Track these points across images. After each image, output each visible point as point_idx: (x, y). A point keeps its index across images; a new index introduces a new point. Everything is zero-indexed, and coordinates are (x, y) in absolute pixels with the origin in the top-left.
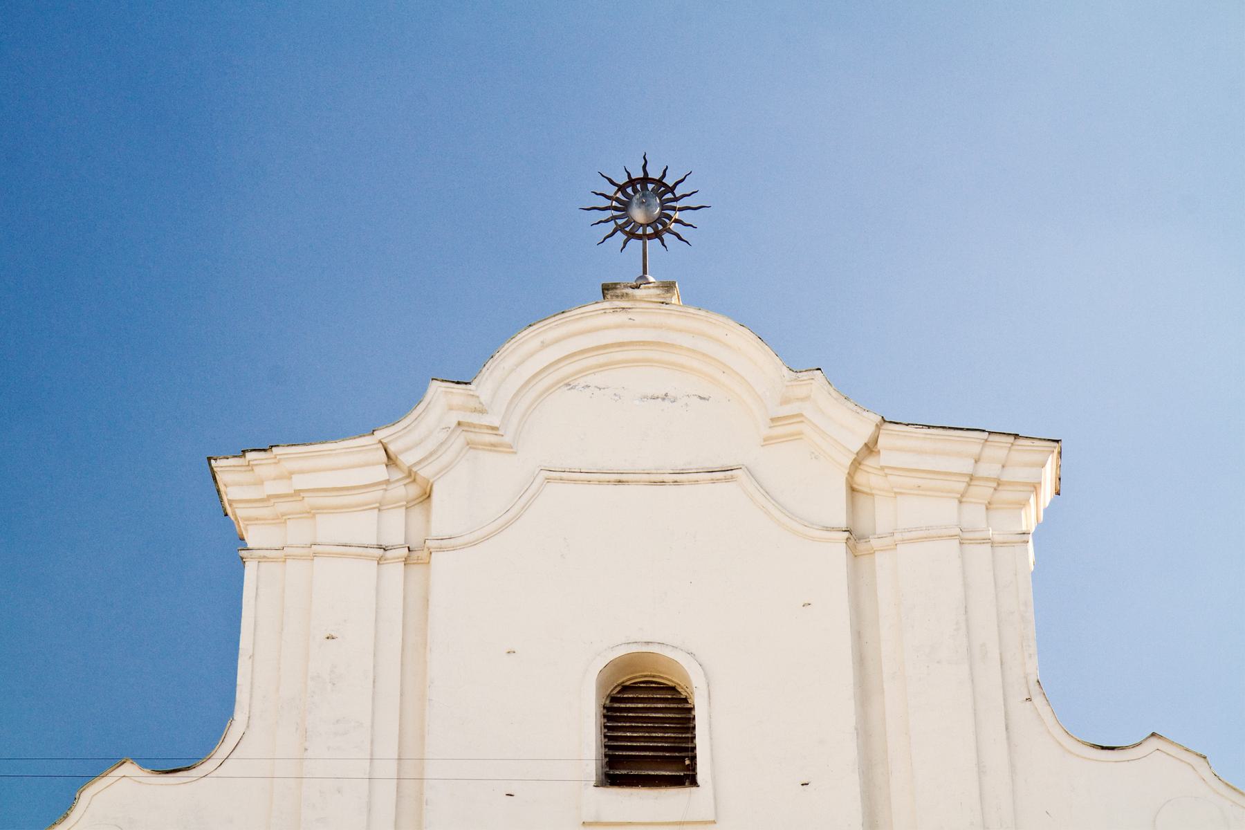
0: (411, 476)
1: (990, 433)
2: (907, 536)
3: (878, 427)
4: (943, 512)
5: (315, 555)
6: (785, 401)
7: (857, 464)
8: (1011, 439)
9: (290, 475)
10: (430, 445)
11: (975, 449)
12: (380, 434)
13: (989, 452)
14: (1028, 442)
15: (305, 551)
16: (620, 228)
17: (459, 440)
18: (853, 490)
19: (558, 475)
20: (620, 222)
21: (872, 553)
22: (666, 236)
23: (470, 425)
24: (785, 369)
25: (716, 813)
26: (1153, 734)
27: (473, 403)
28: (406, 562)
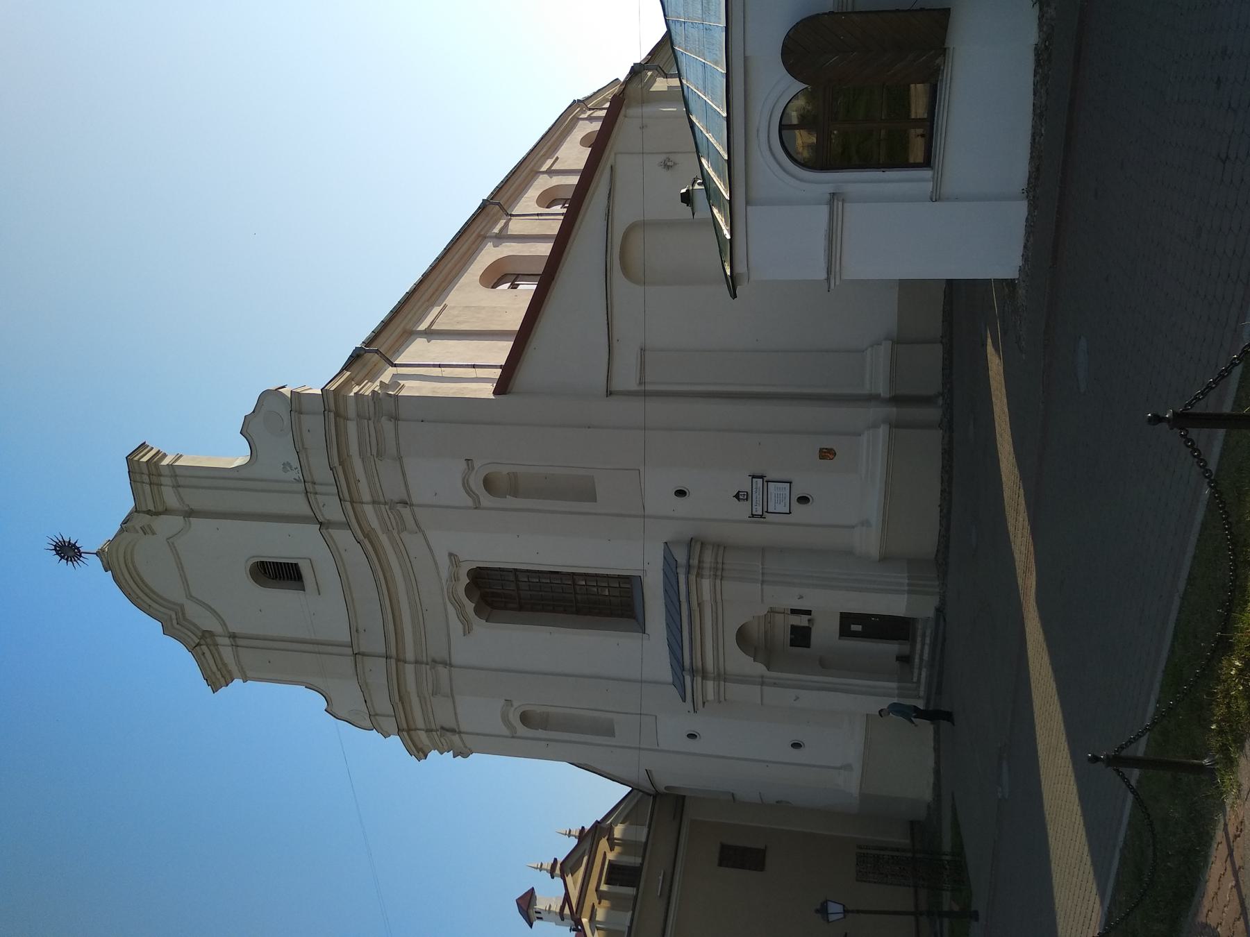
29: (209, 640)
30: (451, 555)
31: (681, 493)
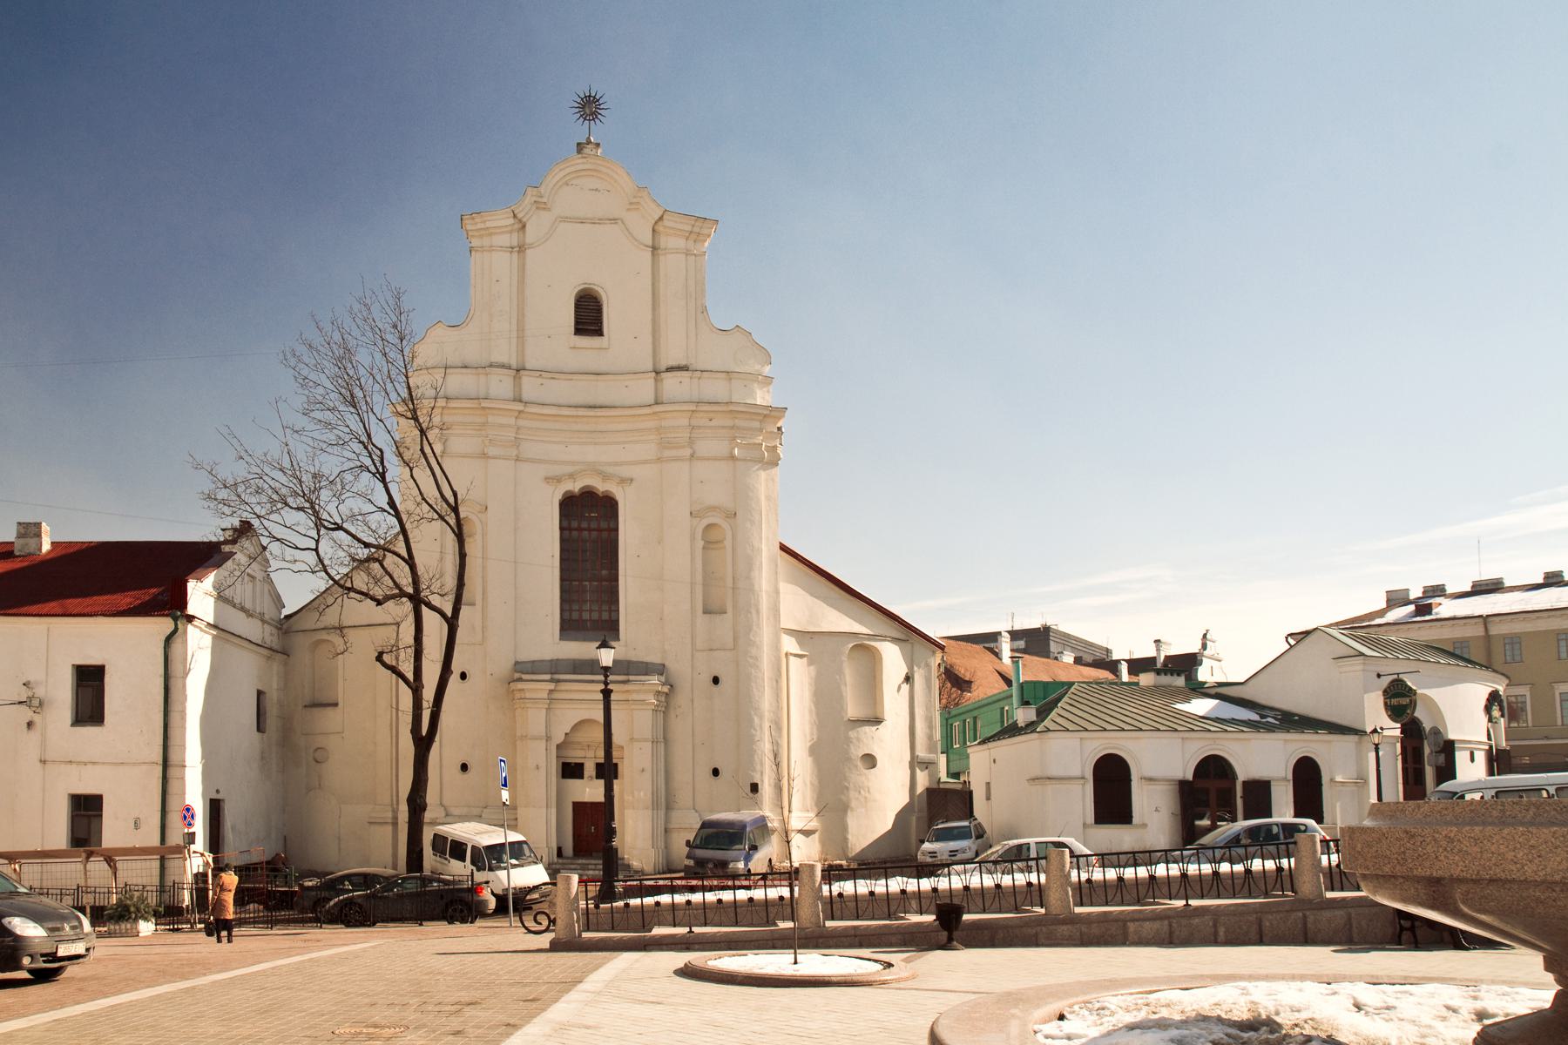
0: (520, 221)
4: (680, 243)
6: (635, 197)
7: (656, 223)
9: (485, 222)
11: (693, 223)
17: (534, 208)
18: (654, 230)
19: (565, 219)
22: (596, 120)
25: (609, 345)
28: (519, 252)
29: (516, 226)
30: (632, 480)
31: (716, 680)
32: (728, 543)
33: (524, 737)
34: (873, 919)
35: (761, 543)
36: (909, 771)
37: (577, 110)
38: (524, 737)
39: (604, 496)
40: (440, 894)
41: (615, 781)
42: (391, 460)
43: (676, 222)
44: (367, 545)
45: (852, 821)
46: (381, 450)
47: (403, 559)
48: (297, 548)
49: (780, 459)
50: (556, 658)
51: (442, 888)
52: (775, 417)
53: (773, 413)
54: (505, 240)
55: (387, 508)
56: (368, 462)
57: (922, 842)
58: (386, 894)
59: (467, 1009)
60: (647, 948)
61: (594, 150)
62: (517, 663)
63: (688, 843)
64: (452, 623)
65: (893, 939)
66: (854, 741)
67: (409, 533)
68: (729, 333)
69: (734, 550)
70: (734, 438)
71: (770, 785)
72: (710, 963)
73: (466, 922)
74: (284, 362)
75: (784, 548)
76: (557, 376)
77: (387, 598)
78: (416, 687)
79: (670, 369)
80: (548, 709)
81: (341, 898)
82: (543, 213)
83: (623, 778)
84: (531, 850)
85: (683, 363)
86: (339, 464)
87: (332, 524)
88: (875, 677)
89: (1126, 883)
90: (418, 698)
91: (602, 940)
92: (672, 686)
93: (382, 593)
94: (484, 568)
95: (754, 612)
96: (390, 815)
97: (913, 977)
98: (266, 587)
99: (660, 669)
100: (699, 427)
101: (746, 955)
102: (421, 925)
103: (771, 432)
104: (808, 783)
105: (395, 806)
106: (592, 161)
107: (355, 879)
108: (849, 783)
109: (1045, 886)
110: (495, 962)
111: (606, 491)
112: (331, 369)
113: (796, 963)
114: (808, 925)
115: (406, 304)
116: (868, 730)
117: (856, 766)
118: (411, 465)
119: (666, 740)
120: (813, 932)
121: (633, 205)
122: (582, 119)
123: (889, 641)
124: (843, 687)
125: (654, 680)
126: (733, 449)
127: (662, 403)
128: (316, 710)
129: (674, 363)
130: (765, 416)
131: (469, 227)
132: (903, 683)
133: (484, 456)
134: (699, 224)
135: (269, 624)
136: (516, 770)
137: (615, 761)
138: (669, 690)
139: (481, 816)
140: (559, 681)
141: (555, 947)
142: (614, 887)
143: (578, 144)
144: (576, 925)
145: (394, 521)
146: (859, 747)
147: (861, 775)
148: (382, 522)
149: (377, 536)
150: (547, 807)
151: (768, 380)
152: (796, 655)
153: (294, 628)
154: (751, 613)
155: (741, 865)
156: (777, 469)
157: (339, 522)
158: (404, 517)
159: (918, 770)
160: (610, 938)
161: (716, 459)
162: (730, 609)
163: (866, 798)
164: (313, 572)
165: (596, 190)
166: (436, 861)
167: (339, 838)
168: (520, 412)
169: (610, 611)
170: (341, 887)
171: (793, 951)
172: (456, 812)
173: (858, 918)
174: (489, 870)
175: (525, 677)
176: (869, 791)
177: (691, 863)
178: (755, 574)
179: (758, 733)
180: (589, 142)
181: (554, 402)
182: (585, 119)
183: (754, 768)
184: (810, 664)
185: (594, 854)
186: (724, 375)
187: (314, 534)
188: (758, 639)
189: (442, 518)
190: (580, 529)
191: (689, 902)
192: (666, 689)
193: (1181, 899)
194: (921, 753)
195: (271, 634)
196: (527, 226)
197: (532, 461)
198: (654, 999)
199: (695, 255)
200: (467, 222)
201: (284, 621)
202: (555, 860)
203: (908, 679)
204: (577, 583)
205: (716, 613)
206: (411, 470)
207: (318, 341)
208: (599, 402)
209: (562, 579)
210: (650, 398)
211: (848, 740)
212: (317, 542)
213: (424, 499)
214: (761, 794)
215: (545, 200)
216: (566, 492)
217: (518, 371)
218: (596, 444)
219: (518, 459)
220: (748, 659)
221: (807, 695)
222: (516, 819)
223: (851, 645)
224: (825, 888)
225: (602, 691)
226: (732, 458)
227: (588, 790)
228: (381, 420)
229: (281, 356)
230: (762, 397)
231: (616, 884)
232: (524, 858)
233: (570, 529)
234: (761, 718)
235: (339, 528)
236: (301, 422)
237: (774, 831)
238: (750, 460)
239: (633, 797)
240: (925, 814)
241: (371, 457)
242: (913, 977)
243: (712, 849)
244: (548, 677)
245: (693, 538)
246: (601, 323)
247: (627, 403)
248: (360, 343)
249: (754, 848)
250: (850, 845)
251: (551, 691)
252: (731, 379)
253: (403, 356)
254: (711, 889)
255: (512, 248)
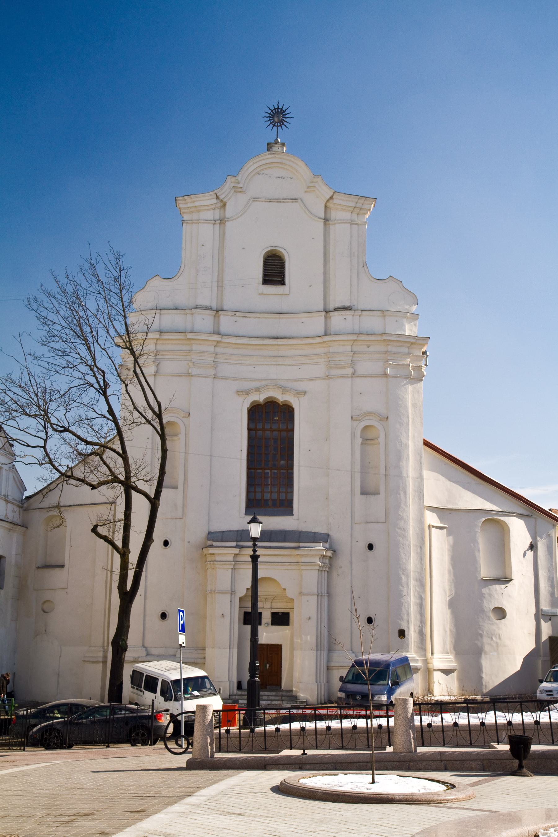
0: (222, 201)
1: (360, 196)
2: (338, 222)
3: (334, 193)
4: (347, 215)
5: (200, 223)
6: (312, 182)
7: (328, 201)
8: (365, 198)
9: (194, 202)
10: (226, 193)
12: (216, 191)
13: (360, 201)
14: (369, 199)
15: (196, 222)
16: (271, 123)
17: (233, 191)
19: (257, 199)
20: (271, 121)
21: (329, 224)
22: (283, 126)
23: (236, 187)
24: (312, 175)
25: (386, 520)
26: (391, 276)
27: (237, 181)
28: (220, 224)
30: (305, 392)
31: (370, 547)
32: (381, 440)
33: (213, 592)
34: (457, 746)
35: (408, 440)
36: (535, 623)
37: (268, 119)
38: (213, 592)
39: (283, 405)
40: (126, 721)
41: (259, 627)
42: (111, 378)
43: (343, 200)
44: (87, 443)
45: (485, 663)
46: (103, 372)
47: (118, 453)
48: (29, 446)
49: (424, 376)
50: (241, 529)
51: (126, 715)
52: (419, 344)
53: (418, 342)
54: (209, 215)
55: (107, 415)
56: (93, 380)
57: (541, 681)
58: (80, 721)
59: (79, 819)
60: (267, 767)
61: (280, 149)
62: (210, 533)
63: (341, 679)
64: (154, 503)
65: (474, 764)
66: (487, 596)
67: (123, 434)
68: (385, 281)
69: (386, 445)
70: (387, 361)
71: (415, 632)
72: (302, 781)
73: (147, 745)
74: (29, 306)
75: (427, 444)
76: (247, 315)
77: (101, 484)
78: (124, 553)
79: (336, 309)
80: (233, 569)
81: (43, 725)
82: (239, 195)
83: (293, 625)
84: (211, 684)
85: (347, 304)
86: (69, 382)
87: (61, 427)
88: (503, 545)
89: (487, 727)
90: (125, 562)
91: (230, 760)
92: (334, 551)
93: (97, 480)
94: (186, 460)
95: (402, 493)
96: (101, 654)
97: (470, 798)
98: (11, 475)
99: (325, 538)
100: (359, 352)
101: (337, 775)
102: (108, 747)
103: (417, 356)
104: (448, 630)
105: (106, 648)
106: (279, 156)
107: (63, 709)
108: (483, 631)
109: (393, 728)
110: (130, 779)
111: (286, 401)
112: (64, 311)
113: (373, 782)
114: (402, 750)
115: (125, 263)
116: (498, 588)
117: (489, 617)
118: (126, 383)
119: (329, 594)
120: (405, 756)
121: (310, 189)
122: (271, 126)
123: (515, 516)
124: (477, 553)
125: (320, 546)
126: (387, 368)
127: (330, 335)
128: (46, 571)
129: (340, 305)
130: (412, 343)
131: (181, 206)
132: (528, 550)
133: (189, 375)
134: (361, 201)
135: (12, 503)
136: (206, 618)
137: (260, 610)
138: (333, 554)
139: (175, 656)
140: (242, 547)
141: (191, 766)
142: (255, 715)
143: (268, 144)
144: (210, 747)
145: (111, 424)
146: (491, 602)
147: (493, 624)
148: (104, 425)
149: (99, 436)
150: (230, 649)
151: (415, 316)
152: (437, 527)
153: (33, 507)
154: (399, 494)
155: (384, 698)
156: (421, 385)
157: (66, 425)
158: (120, 422)
159: (542, 622)
160: (237, 758)
161: (372, 376)
162: (382, 490)
163: (497, 643)
164: (40, 464)
165: (282, 177)
166: (133, 693)
167: (58, 675)
168: (218, 342)
169: (287, 492)
170: (52, 715)
171: (371, 772)
172: (154, 651)
173: (444, 745)
174: (174, 700)
175: (215, 544)
176: (500, 638)
177: (343, 695)
178: (403, 464)
179: (405, 589)
180: (276, 142)
181: (245, 334)
182: (274, 125)
183: (402, 617)
184: (449, 534)
185: (268, 687)
186: (379, 313)
187: (43, 435)
188: (405, 514)
189: (149, 422)
190: (264, 430)
191: (354, 727)
192: (329, 554)
193: (299, 748)
194: (545, 606)
195: (13, 511)
196: (227, 205)
197: (227, 378)
198: (239, 811)
199: (358, 224)
200: (180, 202)
201: (25, 501)
202: (235, 692)
203: (532, 547)
204: (261, 471)
205: (371, 494)
206: (126, 386)
207: (55, 290)
208: (281, 333)
209: (249, 468)
210: (321, 331)
211: (482, 596)
212: (46, 441)
213: (135, 408)
214: (408, 638)
215: (241, 185)
216: (254, 402)
217: (217, 311)
218: (277, 365)
219: (215, 377)
220: (398, 530)
221: (446, 558)
222: (205, 658)
223: (483, 519)
224: (417, 718)
225: (252, 557)
226: (386, 375)
227: (265, 633)
228: (104, 349)
229: (26, 302)
230: (410, 329)
231: (257, 712)
232: (205, 690)
233: (256, 430)
234: (408, 577)
235: (66, 430)
236: (44, 350)
237: (417, 670)
238: (399, 377)
239: (301, 640)
240: (548, 658)
241: (95, 376)
242: (470, 798)
243: (360, 684)
244: (234, 544)
245: (353, 437)
246: (284, 275)
247: (303, 334)
248: (89, 292)
249: (396, 684)
250: (484, 683)
251: (236, 555)
252: (385, 316)
253: (122, 301)
254: (347, 717)
255: (215, 221)
